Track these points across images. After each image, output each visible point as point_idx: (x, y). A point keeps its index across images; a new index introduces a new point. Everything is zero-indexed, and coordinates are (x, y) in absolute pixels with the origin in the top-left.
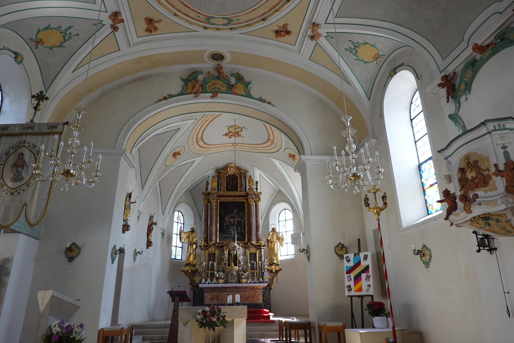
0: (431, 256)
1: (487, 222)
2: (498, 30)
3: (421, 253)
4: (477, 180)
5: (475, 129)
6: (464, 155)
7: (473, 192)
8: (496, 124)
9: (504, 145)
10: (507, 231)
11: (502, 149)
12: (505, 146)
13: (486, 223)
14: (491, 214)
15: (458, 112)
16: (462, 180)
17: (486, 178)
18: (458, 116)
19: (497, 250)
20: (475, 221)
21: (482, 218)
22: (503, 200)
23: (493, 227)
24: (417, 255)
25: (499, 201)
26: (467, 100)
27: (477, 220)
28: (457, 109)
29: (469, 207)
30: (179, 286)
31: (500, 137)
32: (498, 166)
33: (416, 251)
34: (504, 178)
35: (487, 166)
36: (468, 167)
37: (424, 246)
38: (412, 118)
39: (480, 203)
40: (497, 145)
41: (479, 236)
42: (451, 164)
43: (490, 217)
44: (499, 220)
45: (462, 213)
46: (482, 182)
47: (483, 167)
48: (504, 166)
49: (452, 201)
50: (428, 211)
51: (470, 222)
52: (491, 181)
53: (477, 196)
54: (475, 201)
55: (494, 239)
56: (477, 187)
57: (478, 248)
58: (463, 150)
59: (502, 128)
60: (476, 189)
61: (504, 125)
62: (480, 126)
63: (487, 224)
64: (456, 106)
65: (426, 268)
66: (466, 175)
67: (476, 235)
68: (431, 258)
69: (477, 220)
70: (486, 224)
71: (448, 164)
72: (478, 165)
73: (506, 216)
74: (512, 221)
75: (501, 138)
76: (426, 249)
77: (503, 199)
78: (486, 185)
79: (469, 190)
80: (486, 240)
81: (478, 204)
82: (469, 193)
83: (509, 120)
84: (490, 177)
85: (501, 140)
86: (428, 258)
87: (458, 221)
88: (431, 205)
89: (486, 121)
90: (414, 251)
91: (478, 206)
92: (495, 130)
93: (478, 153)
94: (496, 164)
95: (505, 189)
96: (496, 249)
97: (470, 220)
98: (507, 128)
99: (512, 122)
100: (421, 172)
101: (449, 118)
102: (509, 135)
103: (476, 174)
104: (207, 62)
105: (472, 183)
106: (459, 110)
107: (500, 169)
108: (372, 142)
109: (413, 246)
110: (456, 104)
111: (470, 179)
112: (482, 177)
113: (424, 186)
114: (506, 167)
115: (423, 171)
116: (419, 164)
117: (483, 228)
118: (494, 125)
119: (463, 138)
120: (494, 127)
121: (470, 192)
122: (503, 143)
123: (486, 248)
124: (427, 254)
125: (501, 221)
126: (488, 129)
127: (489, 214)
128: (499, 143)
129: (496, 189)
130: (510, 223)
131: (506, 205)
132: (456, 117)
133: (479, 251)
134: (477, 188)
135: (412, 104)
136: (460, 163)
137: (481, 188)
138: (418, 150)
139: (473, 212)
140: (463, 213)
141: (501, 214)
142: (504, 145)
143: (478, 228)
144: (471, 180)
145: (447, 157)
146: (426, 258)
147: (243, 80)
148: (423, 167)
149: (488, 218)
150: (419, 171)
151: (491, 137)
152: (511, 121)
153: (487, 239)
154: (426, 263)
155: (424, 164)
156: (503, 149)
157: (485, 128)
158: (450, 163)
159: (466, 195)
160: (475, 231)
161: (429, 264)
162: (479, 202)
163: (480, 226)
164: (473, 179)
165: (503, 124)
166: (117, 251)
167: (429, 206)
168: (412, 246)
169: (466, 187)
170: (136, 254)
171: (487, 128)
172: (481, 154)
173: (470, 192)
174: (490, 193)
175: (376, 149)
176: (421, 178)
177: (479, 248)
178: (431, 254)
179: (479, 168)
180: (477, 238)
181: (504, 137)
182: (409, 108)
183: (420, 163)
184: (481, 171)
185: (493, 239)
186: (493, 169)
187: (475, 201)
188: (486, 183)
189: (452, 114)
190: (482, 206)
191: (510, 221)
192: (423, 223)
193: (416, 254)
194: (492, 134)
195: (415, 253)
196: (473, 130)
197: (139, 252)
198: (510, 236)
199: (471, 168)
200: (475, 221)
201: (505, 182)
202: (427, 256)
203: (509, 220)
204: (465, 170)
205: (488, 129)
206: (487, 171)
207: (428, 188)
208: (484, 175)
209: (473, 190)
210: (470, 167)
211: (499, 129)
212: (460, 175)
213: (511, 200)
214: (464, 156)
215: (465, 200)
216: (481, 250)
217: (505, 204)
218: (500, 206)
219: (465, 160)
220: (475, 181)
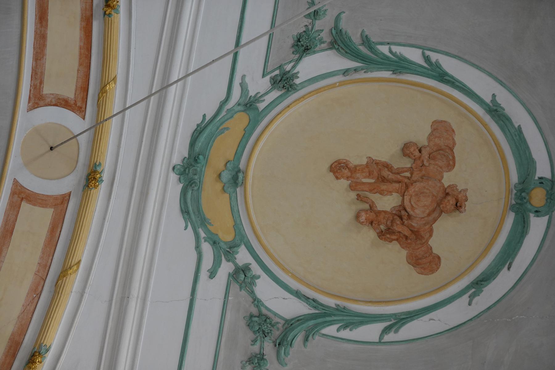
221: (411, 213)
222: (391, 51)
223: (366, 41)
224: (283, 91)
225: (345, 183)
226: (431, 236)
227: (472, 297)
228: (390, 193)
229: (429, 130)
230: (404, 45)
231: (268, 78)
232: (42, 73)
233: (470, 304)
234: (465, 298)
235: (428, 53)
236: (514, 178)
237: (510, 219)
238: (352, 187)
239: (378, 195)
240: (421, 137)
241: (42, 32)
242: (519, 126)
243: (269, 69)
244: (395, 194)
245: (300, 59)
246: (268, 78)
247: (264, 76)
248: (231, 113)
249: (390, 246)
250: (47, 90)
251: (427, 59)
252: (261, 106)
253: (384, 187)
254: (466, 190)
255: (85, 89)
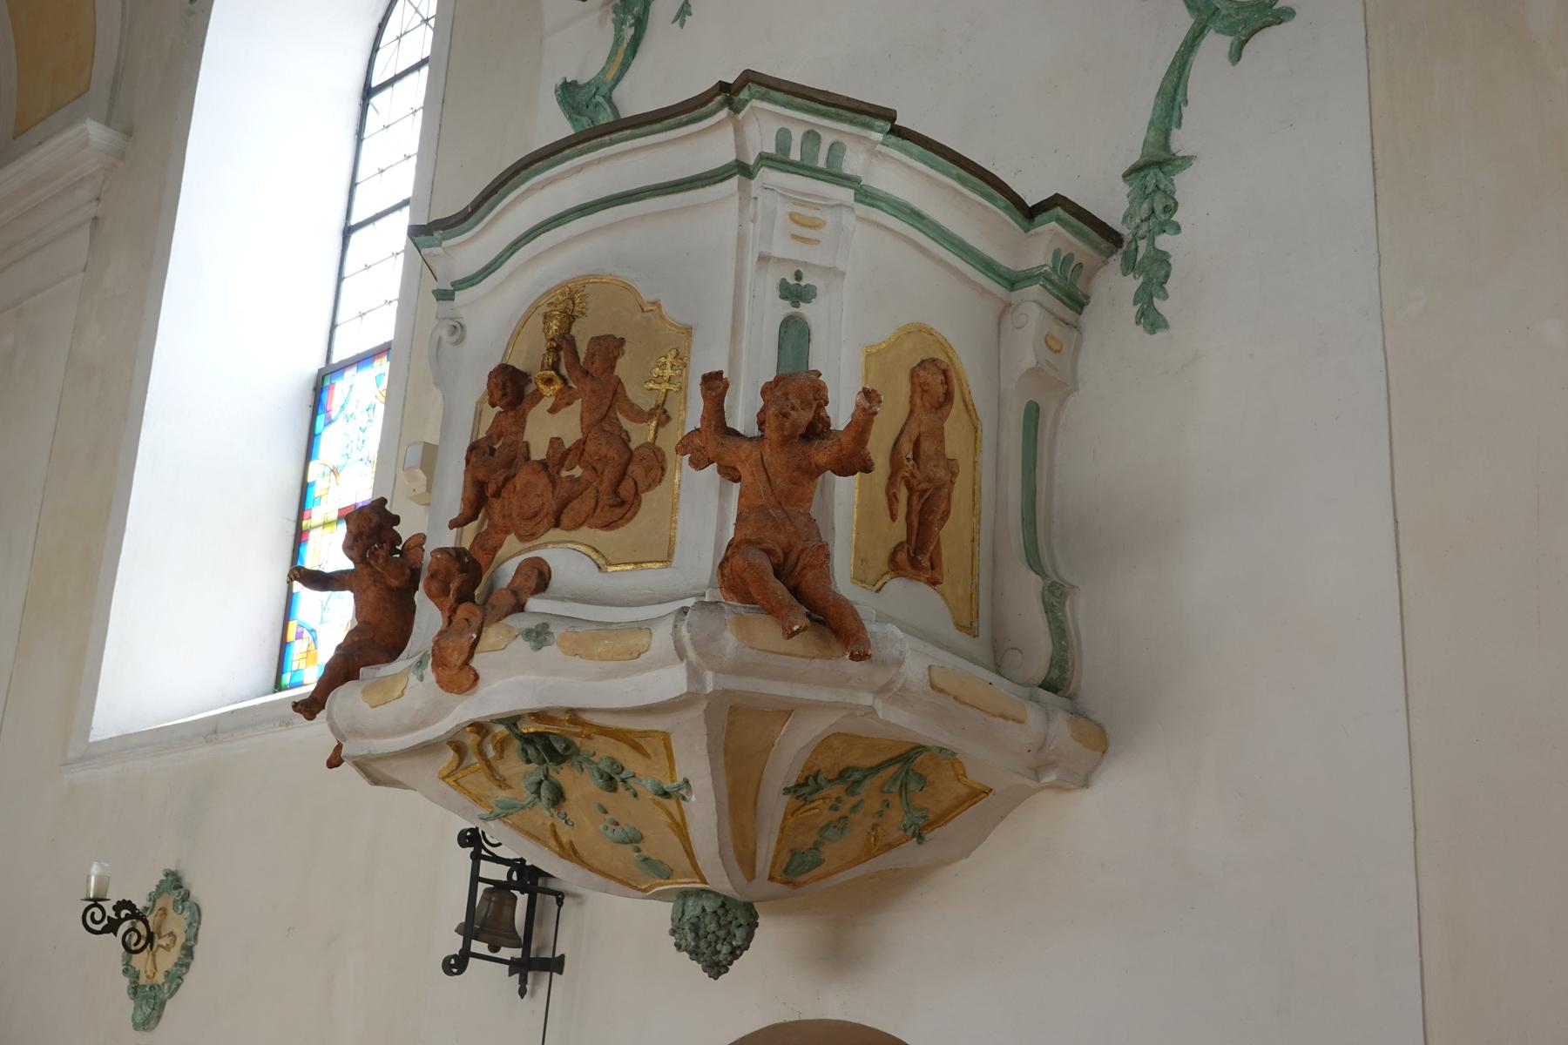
0: (188, 951)
1: (546, 777)
3: (140, 926)
4: (578, 472)
5: (672, 121)
6: (553, 283)
7: (528, 545)
8: (799, 122)
9: (798, 276)
10: (645, 860)
11: (783, 297)
12: (803, 283)
13: (540, 783)
14: (584, 724)
15: (617, 80)
16: (492, 451)
17: (635, 470)
18: (609, 100)
19: (561, 972)
20: (481, 753)
21: (528, 739)
22: (684, 630)
23: (572, 816)
24: (105, 931)
25: (662, 637)
26: (687, 18)
27: (491, 753)
28: (620, 58)
29: (467, 649)
31: (791, 215)
32: (722, 395)
33: (108, 907)
34: (736, 488)
35: (665, 386)
36: (555, 367)
37: (174, 881)
38: (375, 83)
39: (546, 626)
40: (763, 259)
41: (489, 870)
42: (459, 342)
43: (577, 741)
44: (623, 775)
45: (413, 679)
46: (605, 486)
47: (639, 394)
48: (761, 403)
49: (389, 589)
50: (280, 670)
51: (450, 755)
52: (658, 490)
53: (539, 578)
54: (520, 608)
55: (566, 900)
56: (565, 519)
57: (455, 945)
58: (554, 249)
59: (821, 164)
60: (555, 534)
61: (836, 150)
62: (703, 110)
63: (544, 792)
64: (618, 41)
65: (136, 1027)
66: (521, 423)
67: (476, 858)
68: (187, 966)
69: (491, 753)
70: (537, 792)
71: (444, 333)
72: (613, 367)
73: (670, 757)
74: (693, 798)
75: (796, 222)
76: (175, 902)
77: (689, 625)
78: (619, 511)
79: (507, 532)
80: (522, 900)
81: (527, 634)
82: (501, 553)
83: (872, 128)
84: (656, 466)
85: (795, 237)
86: (167, 959)
87: (381, 733)
88: (312, 631)
89: (749, 78)
90: (96, 902)
91: (522, 646)
92: (777, 161)
93: (640, 287)
94: (720, 374)
95: (721, 566)
96: (556, 965)
97: (450, 743)
98: (847, 171)
99: (884, 149)
100: (321, 419)
101: (559, 103)
102: (848, 219)
103: (583, 434)
105: (542, 482)
106: (625, 67)
107: (729, 424)
108: (86, 143)
109: (95, 870)
110: (619, 24)
111: (539, 452)
112: (612, 453)
113: (308, 504)
114: (772, 410)
115: (333, 414)
116: (322, 364)
117: (514, 818)
118: (786, 126)
119: (581, 168)
120: (783, 139)
121: (511, 542)
122: (797, 263)
123: (506, 953)
124: (171, 934)
125: (631, 782)
126: (740, 146)
127: (574, 715)
128: (777, 251)
129: (667, 560)
130: (679, 805)
131: (694, 675)
132: (597, 105)
133: (456, 964)
134: (557, 524)
136: (516, 335)
137: (585, 532)
138: (345, 284)
139: (483, 689)
140: (421, 679)
141: (645, 734)
142: (798, 276)
143: (484, 812)
144: (543, 464)
145: (453, 284)
146: (158, 960)
148: (341, 389)
149: (559, 746)
150: (308, 412)
151: (745, 196)
152: (879, 137)
153: (526, 895)
154: (146, 998)
155: (350, 374)
156: (787, 303)
157: (728, 133)
158: (458, 329)
159: (481, 558)
160: (474, 831)
161: (163, 1004)
162: (539, 621)
163: (503, 795)
164: (560, 455)
167: (299, 636)
168: (90, 865)
169: (496, 504)
171: (738, 131)
172: (654, 303)
173: (511, 542)
174: (623, 578)
175: (98, 199)
176: (309, 455)
177: (467, 945)
178: (196, 936)
179: (615, 393)
180: (475, 878)
181: (814, 225)
182: (378, 19)
183: (335, 360)
184: (620, 416)
185: (560, 897)
186: (693, 414)
187: (520, 608)
188: (623, 503)
189: (582, 81)
190: (551, 652)
191: (683, 792)
192: (215, 732)
193: (98, 928)
194: (755, 184)
195: (98, 916)
196: (656, 126)
198: (650, 897)
199: (565, 381)
200: (481, 753)
201: (733, 519)
202: (167, 948)
203: (679, 788)
204: (530, 389)
205: (740, 146)
206: (654, 424)
207: (325, 524)
208: (626, 442)
209: (533, 536)
210: (564, 371)
211: (806, 163)
212: (490, 414)
213: (730, 641)
214: (548, 292)
215: (459, 590)
216: (471, 959)
217: (690, 667)
218: (654, 674)
219: (547, 317)
220: (564, 474)
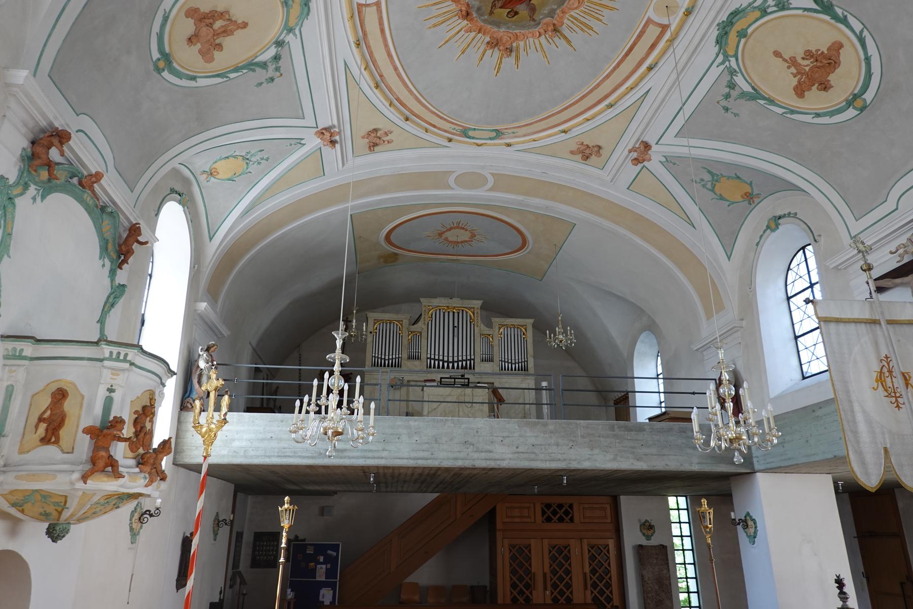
2: (111, 201)
9: (112, 386)
30: (128, 603)
104: (453, 189)
135: (790, 272)
147: (26, 190)
152: (136, 351)
165: (124, 353)
166: (220, 522)
170: (218, 524)
197: (226, 520)
221: (208, 27)
222: (242, 72)
223: (254, 70)
224: (279, 40)
225: (240, 21)
226: (195, 23)
227: (165, 12)
228: (219, 28)
229: (215, 57)
230: (238, 76)
231: (286, 42)
232: (378, 13)
233: (165, 10)
234: (168, 10)
235: (228, 79)
236: (175, 65)
237: (167, 50)
238: (236, 22)
239: (224, 24)
240: (216, 54)
241: (437, 237)
242: (181, 79)
243: (287, 45)
244: (217, 28)
245: (276, 54)
246: (286, 42)
247: (288, 42)
248: (297, 25)
249: (209, 10)
250: (375, 8)
251: (227, 77)
252: (285, 32)
253: (223, 29)
254: (189, 47)
255: (359, 12)
